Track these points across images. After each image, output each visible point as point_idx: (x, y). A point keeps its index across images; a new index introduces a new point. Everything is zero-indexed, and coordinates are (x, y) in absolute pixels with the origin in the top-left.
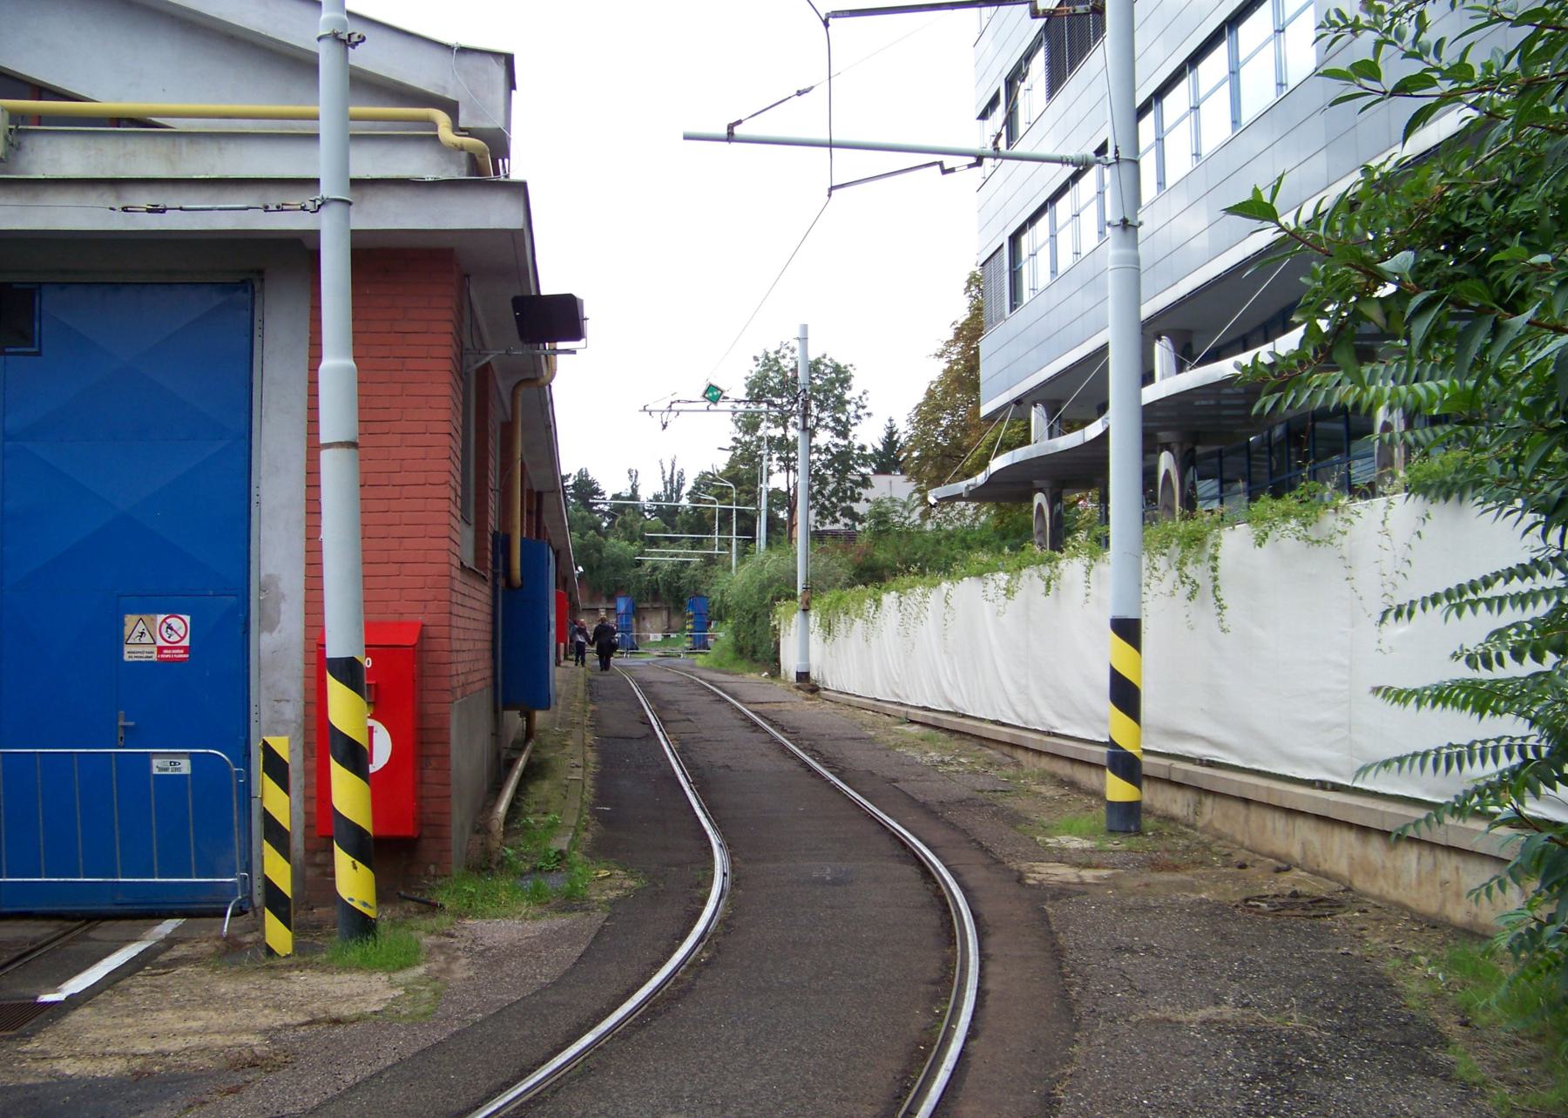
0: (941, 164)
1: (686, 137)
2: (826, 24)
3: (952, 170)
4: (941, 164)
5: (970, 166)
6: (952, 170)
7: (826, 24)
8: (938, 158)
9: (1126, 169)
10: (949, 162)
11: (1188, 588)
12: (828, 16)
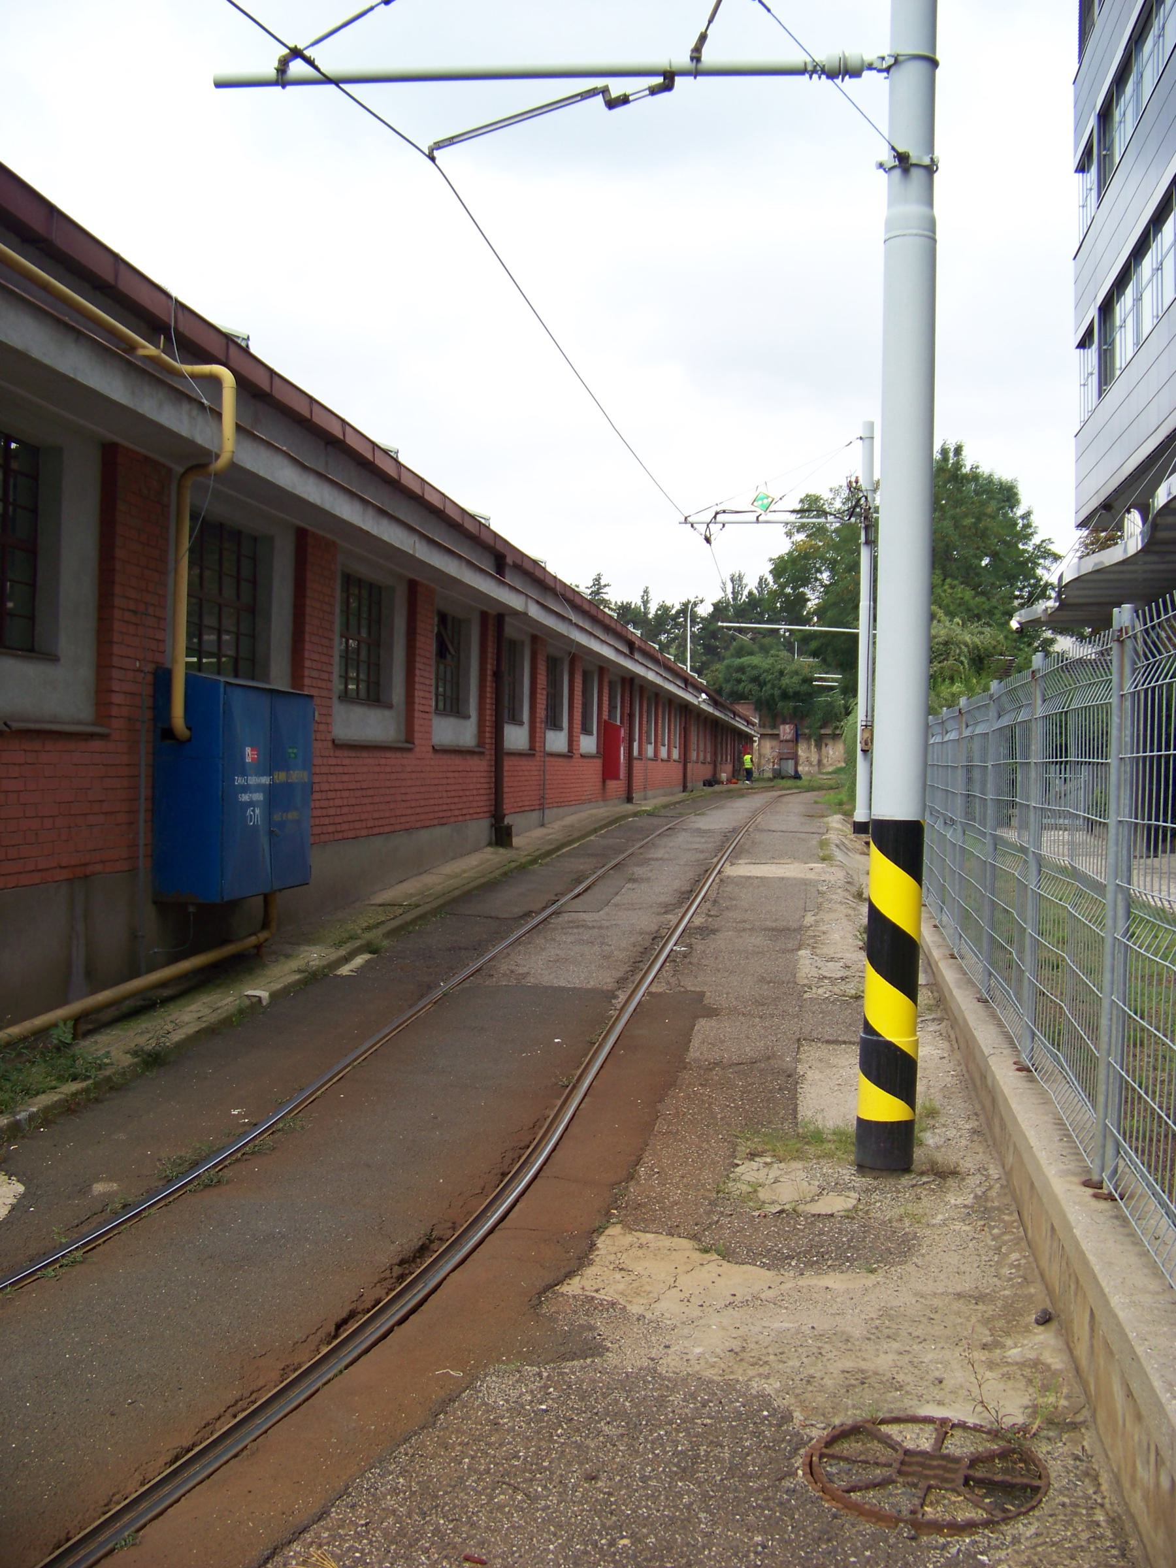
0: (605, 91)
1: (219, 85)
2: (433, 159)
3: (624, 100)
4: (605, 91)
5: (654, 91)
6: (624, 100)
7: (433, 159)
8: (599, 82)
9: (912, 72)
10: (617, 87)
11: (737, 1350)
12: (432, 150)
